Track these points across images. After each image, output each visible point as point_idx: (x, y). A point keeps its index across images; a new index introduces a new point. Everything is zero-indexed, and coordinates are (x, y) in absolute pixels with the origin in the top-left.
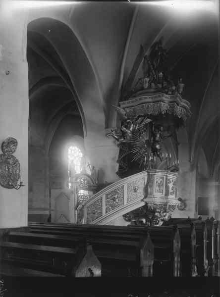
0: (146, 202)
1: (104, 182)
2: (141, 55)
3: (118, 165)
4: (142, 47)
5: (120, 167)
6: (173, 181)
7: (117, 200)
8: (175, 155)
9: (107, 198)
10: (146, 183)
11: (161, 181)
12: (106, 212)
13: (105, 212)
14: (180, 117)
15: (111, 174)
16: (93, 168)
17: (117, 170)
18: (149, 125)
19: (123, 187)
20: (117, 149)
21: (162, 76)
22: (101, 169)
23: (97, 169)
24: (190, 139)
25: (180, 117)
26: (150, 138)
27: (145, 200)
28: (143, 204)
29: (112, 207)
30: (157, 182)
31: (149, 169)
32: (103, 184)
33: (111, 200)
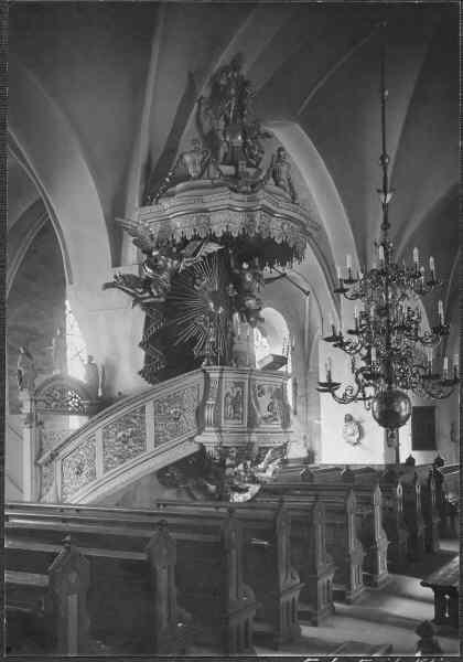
0: (201, 444)
1: (116, 394)
2: (190, 96)
3: (143, 353)
4: (191, 75)
5: (148, 359)
6: (270, 389)
7: (131, 443)
8: (336, 314)
9: (106, 436)
10: (201, 398)
11: (238, 393)
12: (106, 469)
13: (102, 469)
14: (279, 242)
15: (129, 378)
16: (90, 358)
17: (141, 366)
18: (216, 258)
19: (143, 410)
20: (139, 315)
21: (240, 145)
22: (107, 360)
23: (99, 361)
24: (188, 323)
25: (279, 242)
26: (223, 285)
27: (199, 439)
28: (193, 449)
29: (120, 457)
30: (227, 395)
31: (208, 364)
32: (111, 399)
33: (117, 441)
